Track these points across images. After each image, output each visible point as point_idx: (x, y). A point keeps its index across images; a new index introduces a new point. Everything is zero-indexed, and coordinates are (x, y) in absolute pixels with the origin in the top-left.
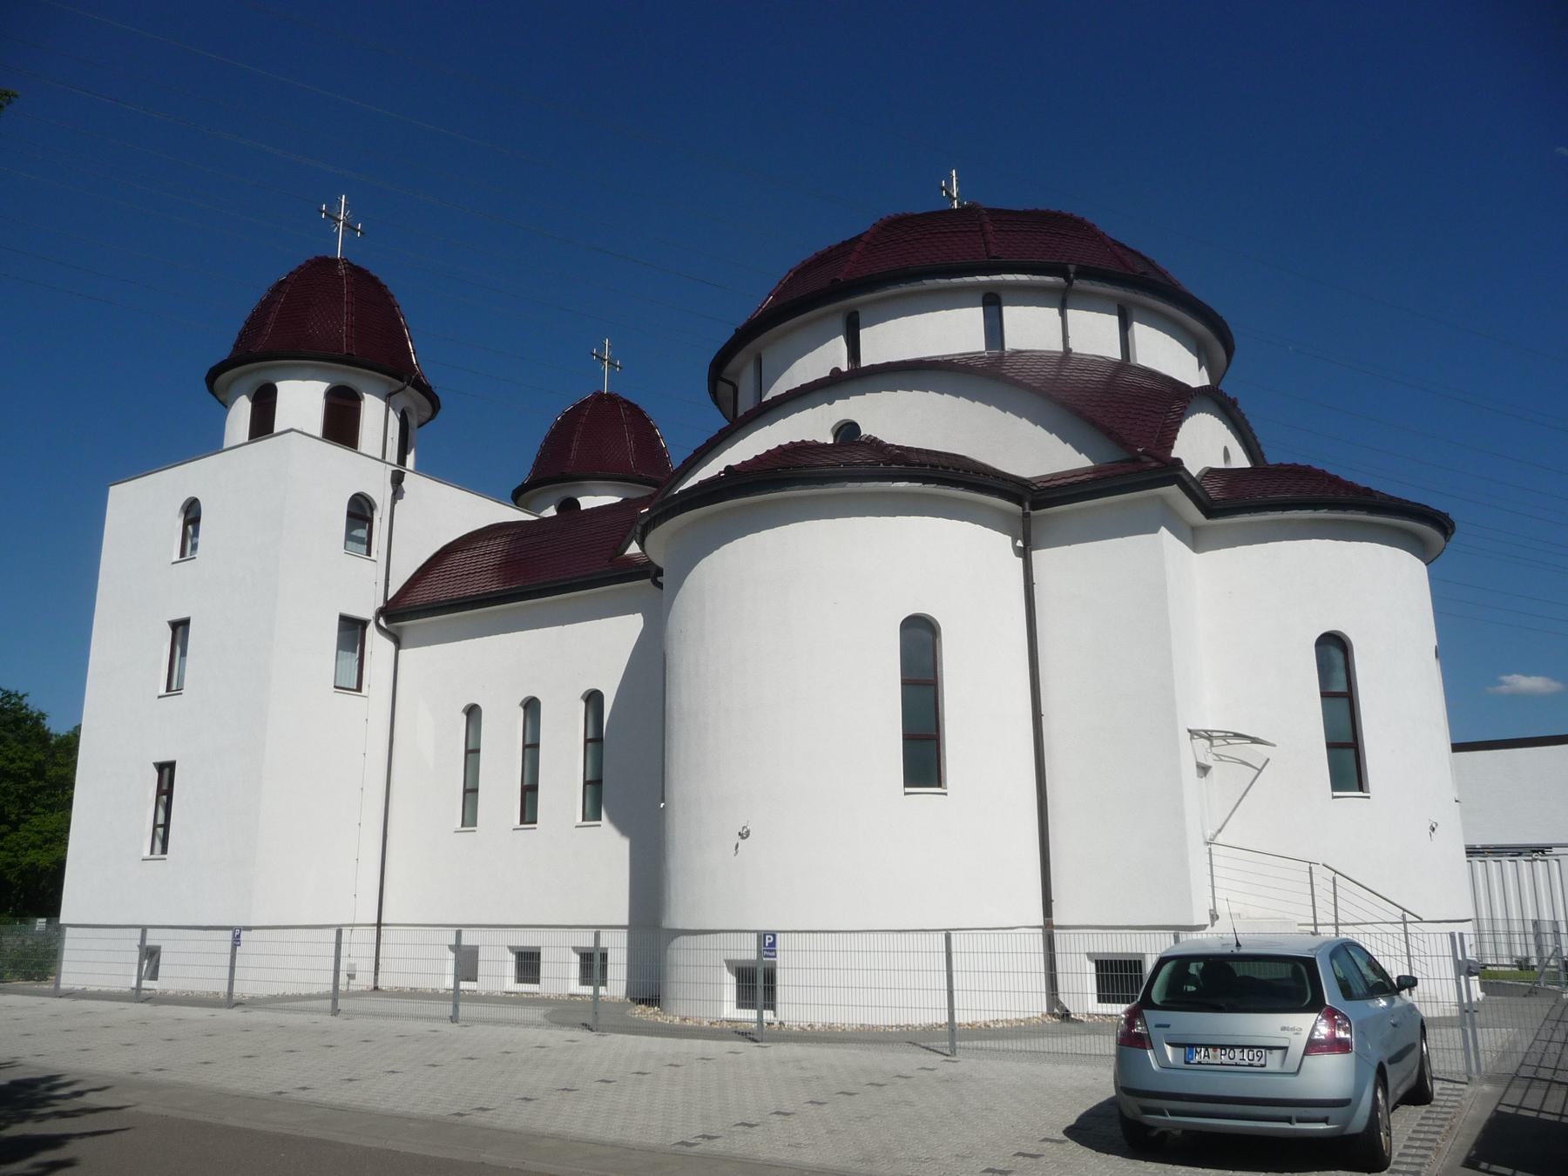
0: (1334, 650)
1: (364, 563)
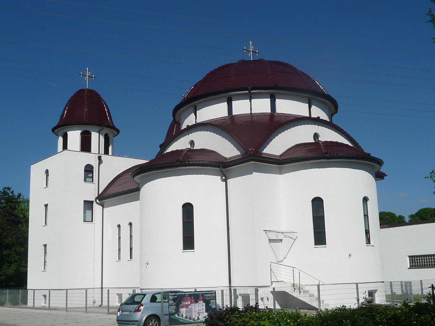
0: (318, 204)
1: (91, 185)
